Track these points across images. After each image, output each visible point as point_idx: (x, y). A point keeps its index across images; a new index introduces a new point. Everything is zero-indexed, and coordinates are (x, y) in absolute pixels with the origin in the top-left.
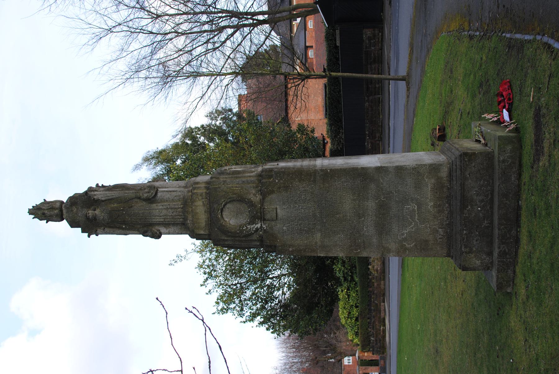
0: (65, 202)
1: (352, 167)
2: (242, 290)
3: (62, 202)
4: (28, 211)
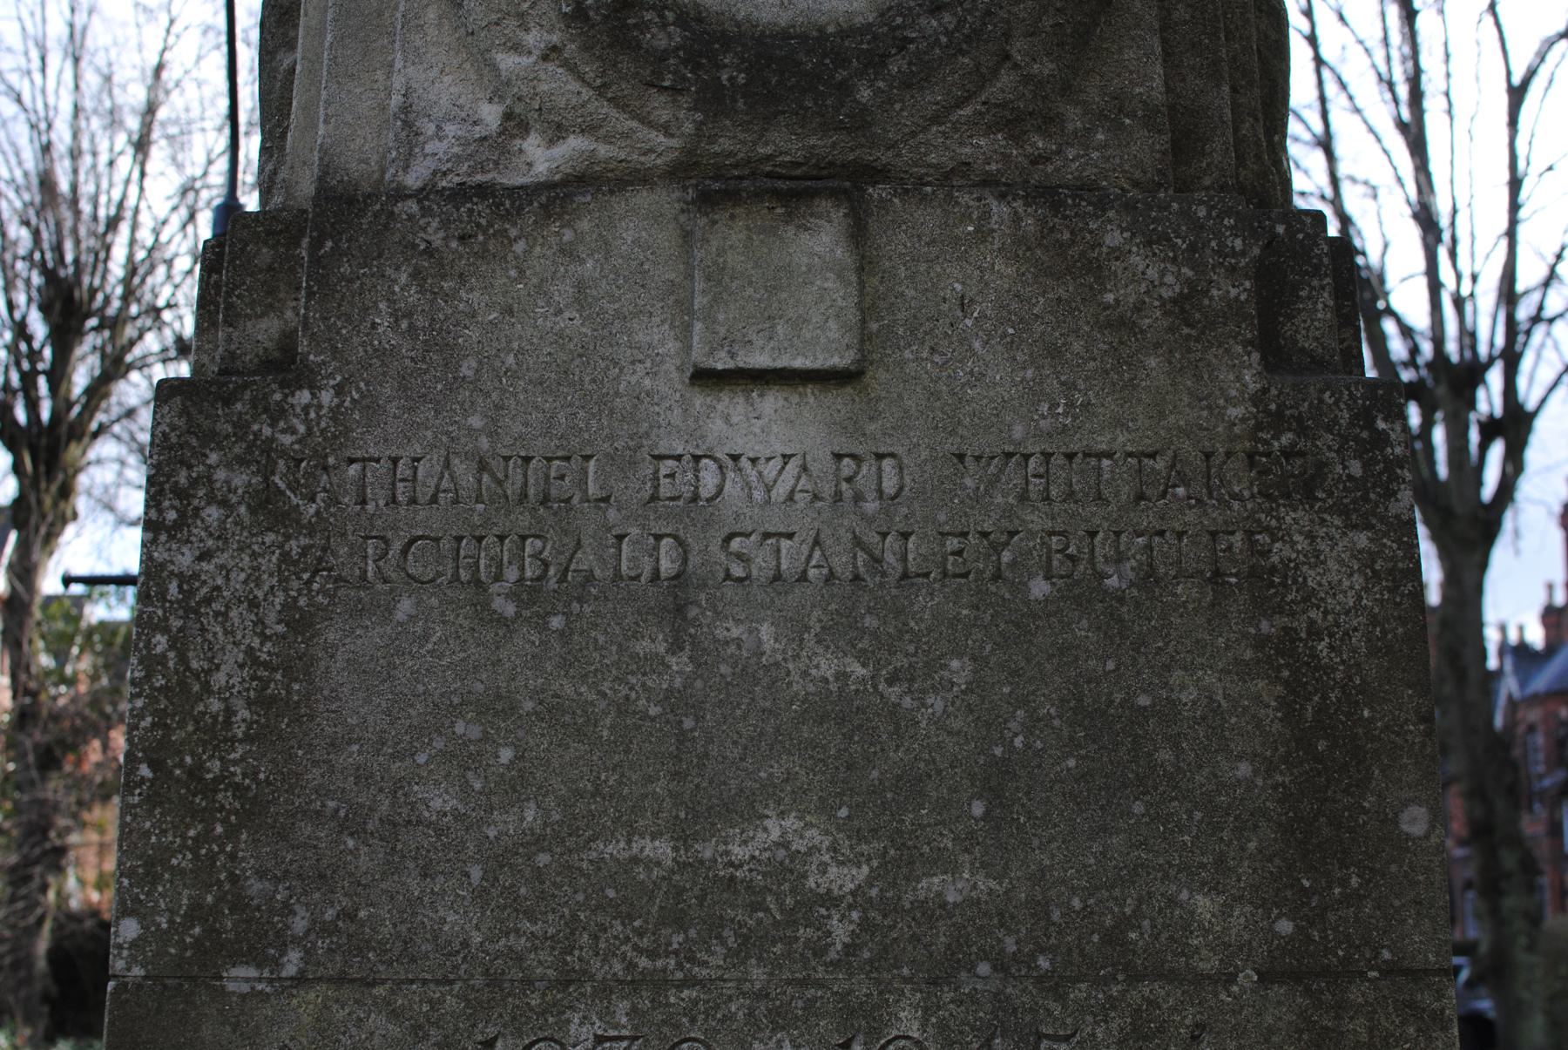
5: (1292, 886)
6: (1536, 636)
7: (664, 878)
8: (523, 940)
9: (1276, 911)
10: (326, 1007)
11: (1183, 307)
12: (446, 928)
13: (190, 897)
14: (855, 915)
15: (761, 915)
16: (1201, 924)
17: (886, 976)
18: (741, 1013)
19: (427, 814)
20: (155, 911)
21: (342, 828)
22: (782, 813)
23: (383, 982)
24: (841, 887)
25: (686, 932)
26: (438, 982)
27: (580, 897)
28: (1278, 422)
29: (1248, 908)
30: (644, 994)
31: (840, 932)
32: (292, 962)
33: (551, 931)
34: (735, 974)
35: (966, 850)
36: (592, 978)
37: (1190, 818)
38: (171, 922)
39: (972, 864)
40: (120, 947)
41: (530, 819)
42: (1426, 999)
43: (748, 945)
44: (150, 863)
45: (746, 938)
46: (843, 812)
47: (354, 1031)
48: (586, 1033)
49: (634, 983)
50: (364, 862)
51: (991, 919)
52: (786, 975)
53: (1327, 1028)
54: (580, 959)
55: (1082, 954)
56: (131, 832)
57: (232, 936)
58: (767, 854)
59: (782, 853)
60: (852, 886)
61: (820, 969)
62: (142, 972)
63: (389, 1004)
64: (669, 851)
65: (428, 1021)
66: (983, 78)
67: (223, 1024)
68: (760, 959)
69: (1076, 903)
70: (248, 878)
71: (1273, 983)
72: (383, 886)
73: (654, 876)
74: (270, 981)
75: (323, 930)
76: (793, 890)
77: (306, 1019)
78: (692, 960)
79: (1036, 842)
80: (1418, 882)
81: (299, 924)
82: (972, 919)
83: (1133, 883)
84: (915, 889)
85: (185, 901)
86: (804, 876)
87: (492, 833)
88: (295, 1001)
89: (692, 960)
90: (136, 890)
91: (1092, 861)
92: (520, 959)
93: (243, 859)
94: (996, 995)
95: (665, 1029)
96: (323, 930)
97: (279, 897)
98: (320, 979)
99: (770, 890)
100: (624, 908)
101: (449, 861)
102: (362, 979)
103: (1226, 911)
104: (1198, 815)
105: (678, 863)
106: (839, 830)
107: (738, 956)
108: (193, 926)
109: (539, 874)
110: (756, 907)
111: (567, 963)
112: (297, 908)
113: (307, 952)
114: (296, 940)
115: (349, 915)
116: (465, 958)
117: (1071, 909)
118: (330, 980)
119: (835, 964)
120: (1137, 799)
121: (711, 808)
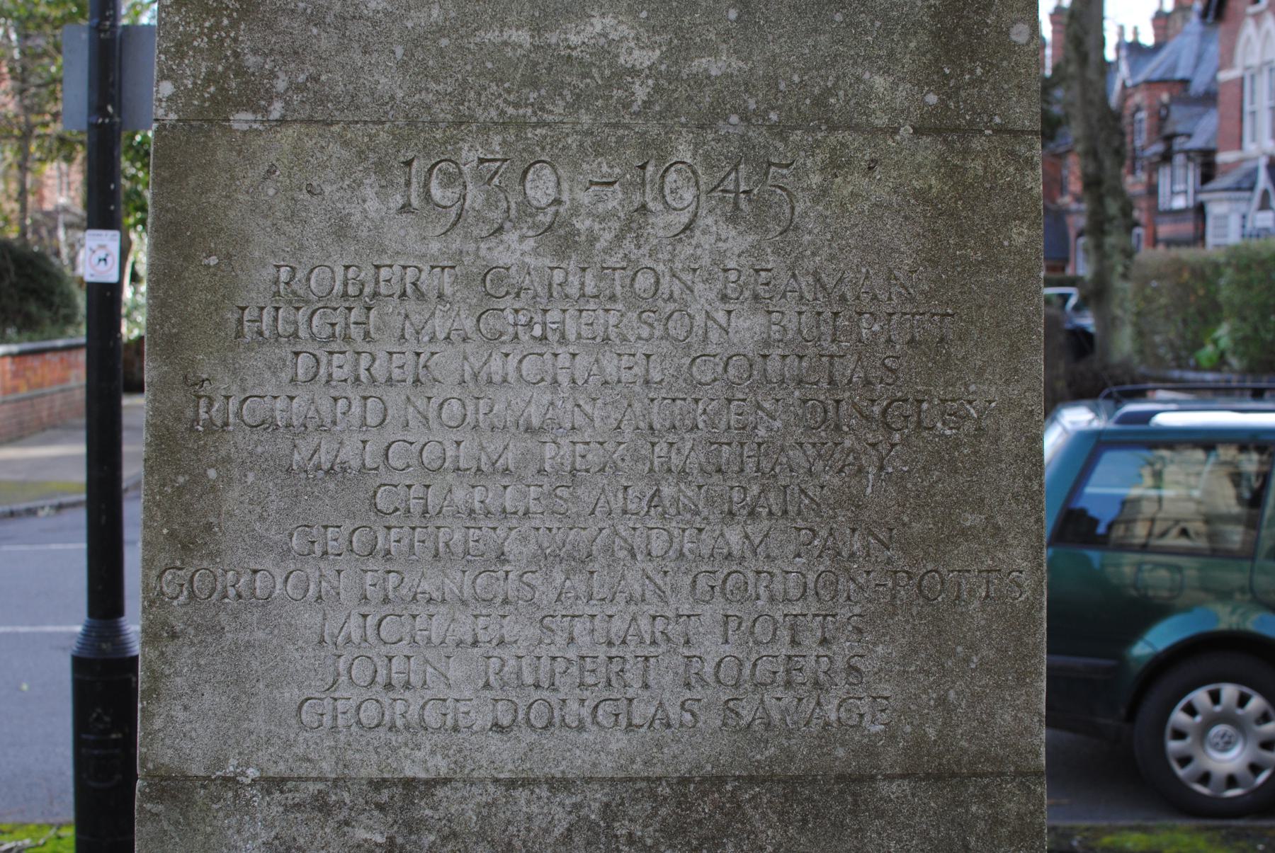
5: (938, 72)
6: (1148, 39)
7: (524, 56)
8: (431, 95)
9: (926, 89)
10: (299, 139)
12: (379, 87)
13: (207, 67)
14: (650, 82)
15: (588, 80)
16: (877, 94)
17: (670, 122)
18: (574, 145)
19: (366, 12)
20: (183, 76)
21: (309, 21)
22: (603, 14)
23: (338, 123)
24: (641, 64)
25: (539, 91)
26: (374, 123)
27: (469, 67)
29: (909, 86)
30: (511, 131)
31: (640, 93)
32: (277, 110)
33: (450, 90)
34: (571, 119)
35: (724, 41)
36: (476, 120)
37: (873, 25)
38: (194, 83)
39: (728, 51)
40: (160, 100)
41: (435, 15)
42: (1022, 149)
43: (580, 100)
44: (179, 45)
45: (579, 96)
46: (644, 14)
47: (319, 155)
48: (473, 156)
50: (324, 44)
51: (740, 87)
52: (605, 120)
53: (956, 166)
54: (468, 108)
55: (799, 110)
56: (165, 24)
57: (236, 92)
58: (593, 41)
59: (602, 41)
60: (649, 63)
61: (627, 116)
62: (176, 117)
63: (342, 137)
64: (528, 38)
65: (368, 148)
67: (231, 151)
68: (587, 109)
69: (796, 78)
70: (245, 54)
71: (923, 135)
72: (337, 59)
73: (518, 55)
74: (262, 122)
75: (297, 88)
76: (610, 65)
77: (286, 147)
78: (542, 109)
79: (770, 38)
80: (1021, 73)
81: (281, 85)
82: (727, 87)
83: (834, 66)
84: (689, 66)
85: (204, 70)
86: (617, 56)
87: (410, 24)
88: (279, 136)
89: (542, 109)
90: (170, 63)
91: (807, 51)
92: (429, 107)
93: (242, 42)
94: (742, 136)
95: (525, 155)
96: (297, 88)
97: (267, 67)
98: (295, 121)
99: (594, 65)
100: (498, 75)
101: (381, 43)
102: (323, 121)
103: (894, 87)
104: (878, 24)
105: (534, 46)
106: (641, 26)
107: (573, 107)
108: (209, 86)
109: (441, 52)
110: (584, 76)
111: (459, 110)
112: (279, 74)
113: (287, 103)
114: (279, 95)
115: (316, 79)
116: (392, 107)
117: (792, 82)
118: (302, 121)
119: (637, 114)
120: (837, 11)
121: (556, 9)
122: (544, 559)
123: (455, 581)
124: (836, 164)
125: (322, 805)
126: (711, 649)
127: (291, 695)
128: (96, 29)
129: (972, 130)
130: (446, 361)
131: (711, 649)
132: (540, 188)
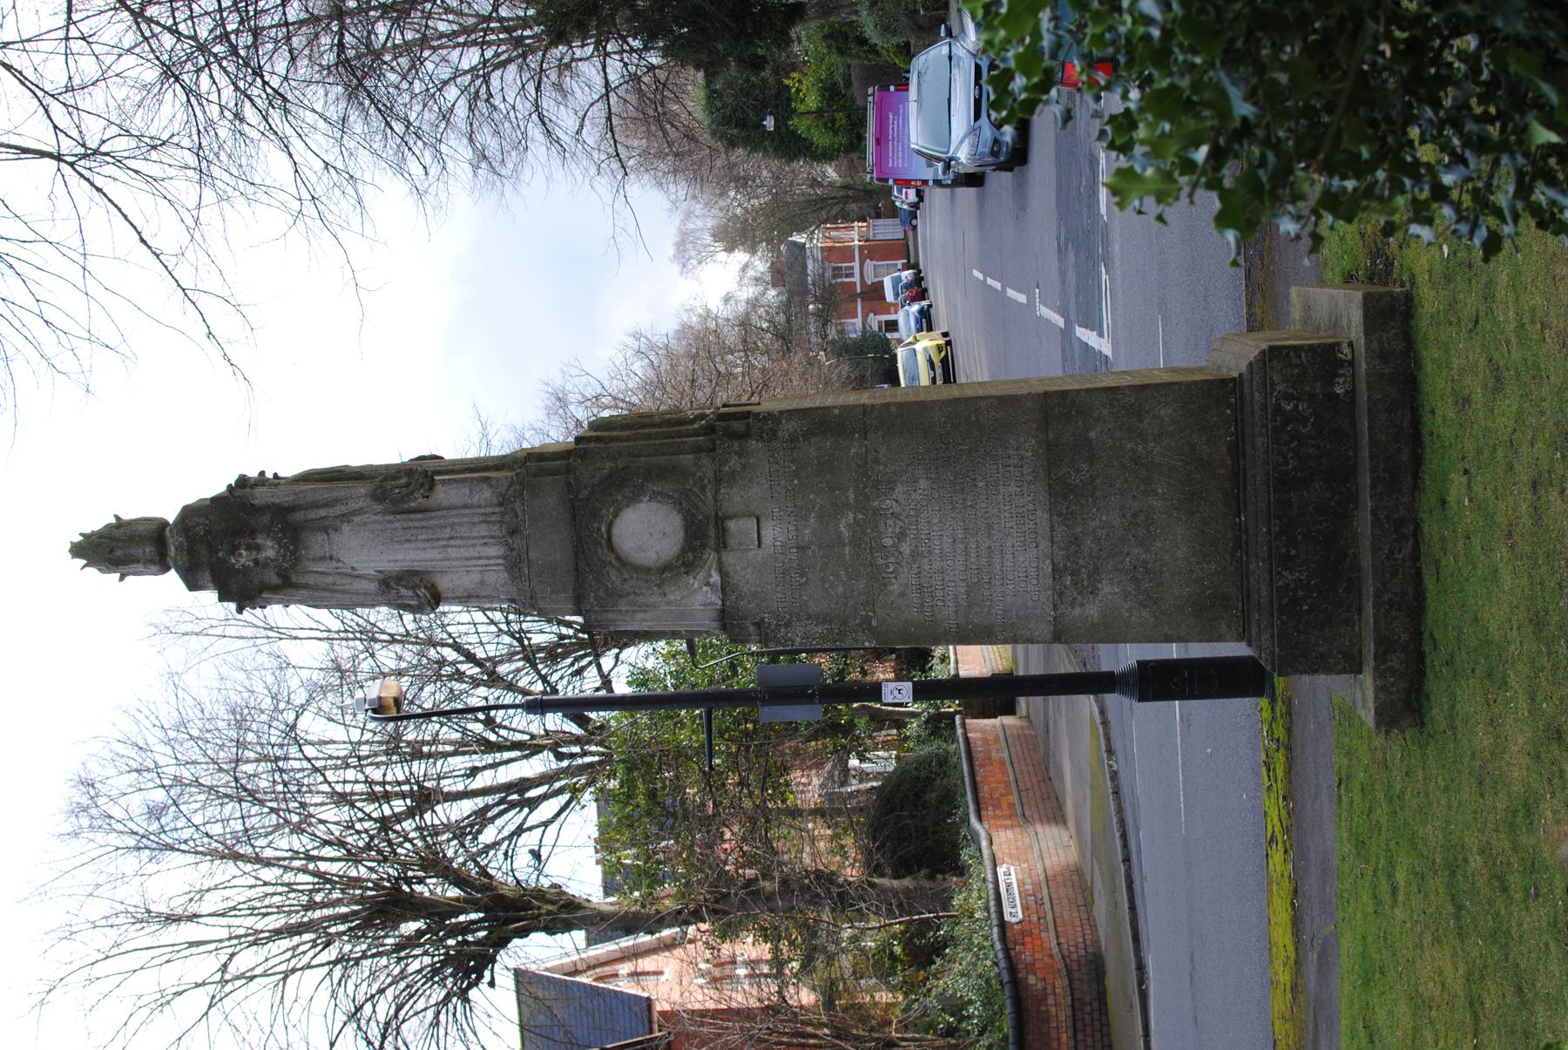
0: (171, 522)
1: (1041, 389)
2: (1198, 180)
3: (163, 524)
4: (69, 546)
11: (740, 456)
28: (762, 437)
32: (871, 614)
43: (863, 533)
49: (871, 552)
66: (695, 494)
107: (866, 534)
122: (989, 536)
123: (997, 560)
124: (877, 462)
125: (1061, 594)
126: (1013, 489)
127: (1030, 603)
128: (765, 702)
129: (864, 423)
130: (936, 566)
131: (1013, 489)
132: (888, 542)
